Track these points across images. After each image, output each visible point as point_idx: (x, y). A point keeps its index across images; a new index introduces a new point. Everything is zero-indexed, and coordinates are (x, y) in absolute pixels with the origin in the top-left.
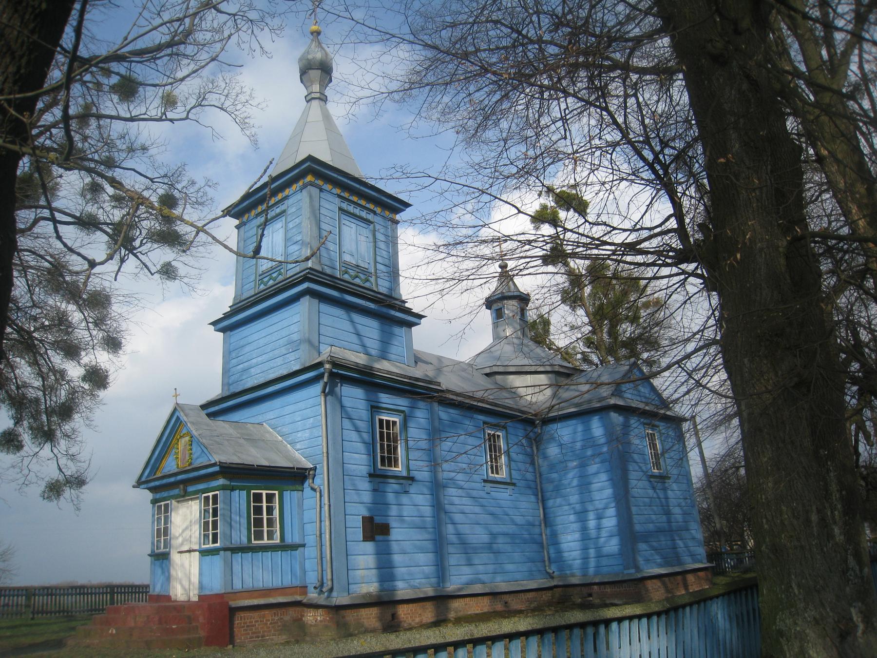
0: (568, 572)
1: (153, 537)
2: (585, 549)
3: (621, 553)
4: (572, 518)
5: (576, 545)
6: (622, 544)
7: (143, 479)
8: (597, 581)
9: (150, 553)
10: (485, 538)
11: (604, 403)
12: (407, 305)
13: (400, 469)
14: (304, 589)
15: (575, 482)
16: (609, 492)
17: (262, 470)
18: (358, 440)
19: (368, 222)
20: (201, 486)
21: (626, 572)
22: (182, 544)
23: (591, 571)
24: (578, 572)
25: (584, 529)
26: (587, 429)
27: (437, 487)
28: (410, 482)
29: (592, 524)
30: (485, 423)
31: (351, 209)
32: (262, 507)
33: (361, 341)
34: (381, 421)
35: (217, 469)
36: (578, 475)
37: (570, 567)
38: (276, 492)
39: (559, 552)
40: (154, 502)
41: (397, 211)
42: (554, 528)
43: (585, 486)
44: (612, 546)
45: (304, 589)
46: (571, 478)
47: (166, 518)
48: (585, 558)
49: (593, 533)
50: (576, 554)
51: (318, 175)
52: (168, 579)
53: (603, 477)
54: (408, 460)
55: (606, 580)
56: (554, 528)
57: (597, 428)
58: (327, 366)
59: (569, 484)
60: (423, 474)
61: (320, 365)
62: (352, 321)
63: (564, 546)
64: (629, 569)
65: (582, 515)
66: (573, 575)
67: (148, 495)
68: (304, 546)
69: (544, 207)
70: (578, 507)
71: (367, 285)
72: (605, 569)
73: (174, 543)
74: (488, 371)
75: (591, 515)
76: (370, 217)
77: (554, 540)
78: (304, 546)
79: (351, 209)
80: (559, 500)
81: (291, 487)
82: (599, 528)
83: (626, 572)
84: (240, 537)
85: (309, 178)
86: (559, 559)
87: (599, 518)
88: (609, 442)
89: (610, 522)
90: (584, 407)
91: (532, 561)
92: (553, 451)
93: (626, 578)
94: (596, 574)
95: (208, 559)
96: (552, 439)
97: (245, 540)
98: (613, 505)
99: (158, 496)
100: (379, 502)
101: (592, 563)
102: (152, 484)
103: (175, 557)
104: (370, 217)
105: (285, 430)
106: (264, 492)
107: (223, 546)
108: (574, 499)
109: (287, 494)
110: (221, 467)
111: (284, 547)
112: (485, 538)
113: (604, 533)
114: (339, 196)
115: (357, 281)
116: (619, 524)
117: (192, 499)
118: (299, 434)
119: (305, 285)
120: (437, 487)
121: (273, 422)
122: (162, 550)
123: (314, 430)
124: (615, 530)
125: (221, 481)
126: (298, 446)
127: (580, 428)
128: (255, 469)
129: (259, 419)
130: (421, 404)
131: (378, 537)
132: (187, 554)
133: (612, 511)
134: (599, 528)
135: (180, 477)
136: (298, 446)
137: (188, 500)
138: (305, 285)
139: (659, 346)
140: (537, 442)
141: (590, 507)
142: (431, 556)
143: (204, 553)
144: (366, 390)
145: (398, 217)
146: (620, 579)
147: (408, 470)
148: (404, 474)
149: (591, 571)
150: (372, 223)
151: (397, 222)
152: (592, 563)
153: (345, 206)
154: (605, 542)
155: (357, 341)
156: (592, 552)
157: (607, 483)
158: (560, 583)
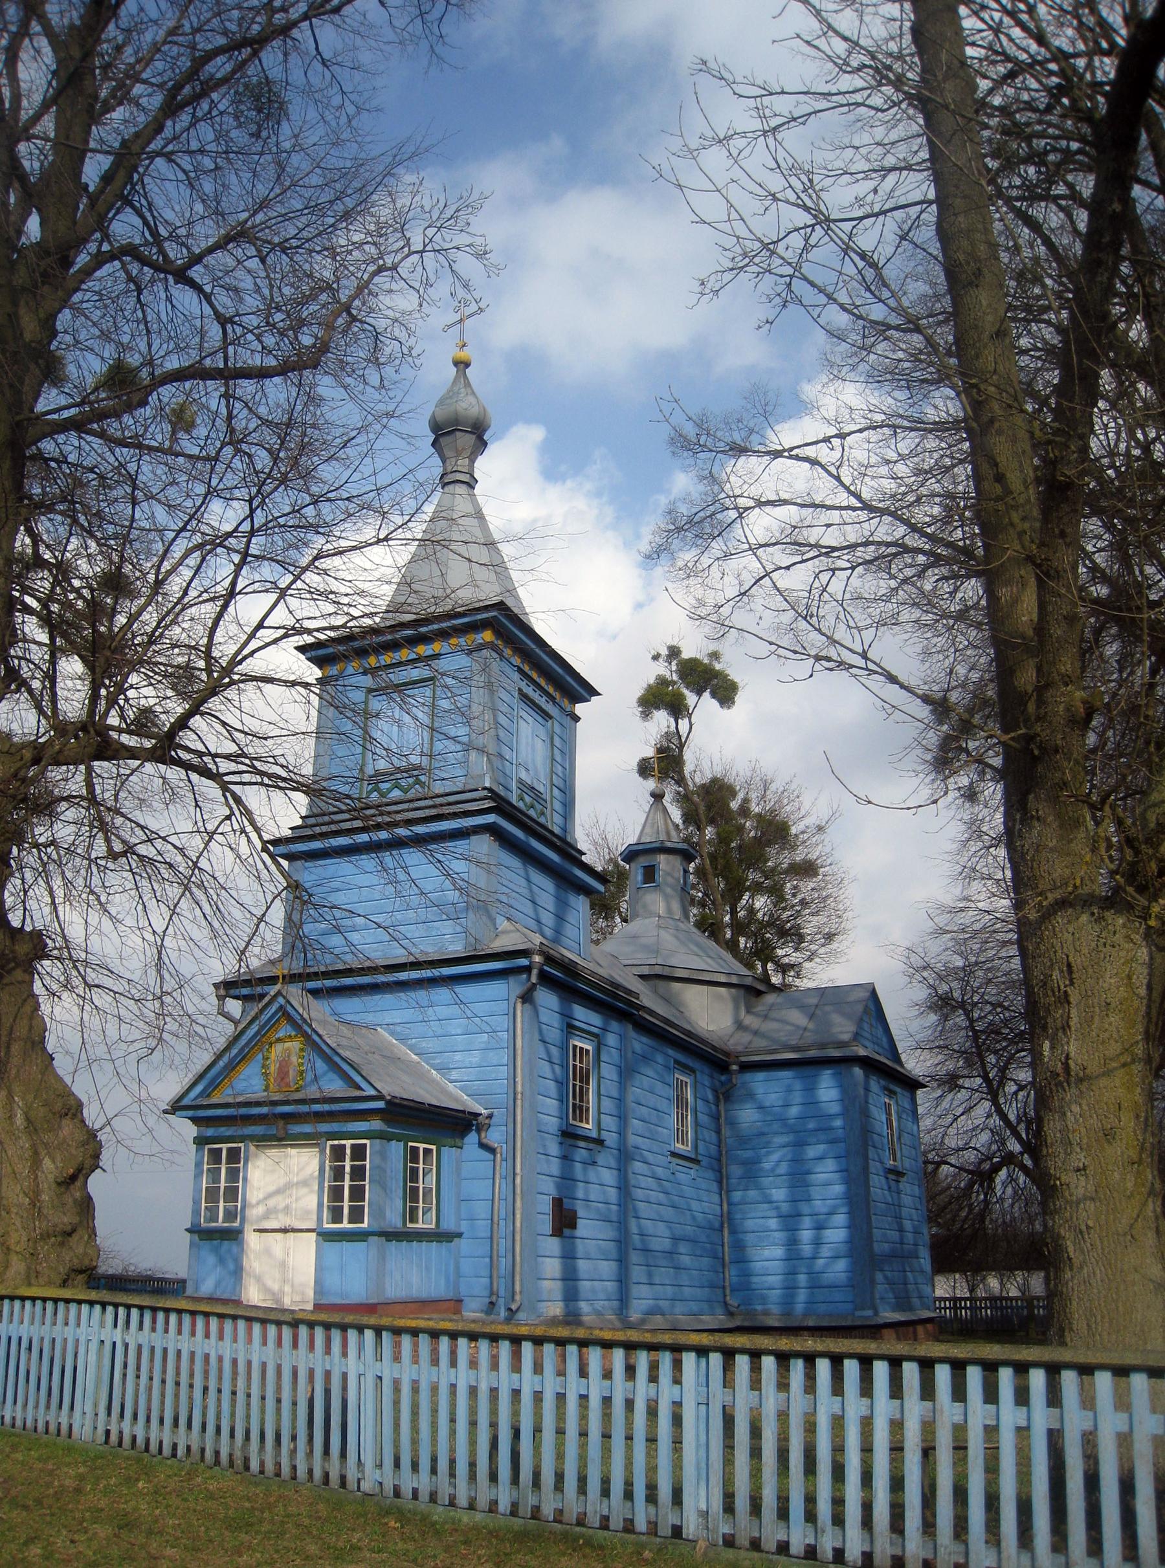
0: (759, 1308)
1: (196, 1202)
2: (791, 1273)
3: (851, 1285)
4: (773, 1223)
5: (777, 1266)
6: (852, 1270)
7: (185, 1102)
8: (811, 1323)
9: (189, 1226)
10: (666, 1244)
11: (846, 1052)
12: (583, 858)
13: (589, 1126)
14: (456, 1304)
15: (783, 1168)
16: (838, 1189)
17: (405, 1106)
18: (549, 1075)
19: (546, 716)
20: (335, 1127)
21: (858, 1313)
22: (266, 1216)
23: (799, 1308)
24: (775, 1309)
25: (792, 1243)
26: (810, 1089)
27: (625, 1156)
28: (599, 1148)
29: (806, 1235)
30: (677, 1062)
31: (536, 696)
32: (352, 1159)
33: (535, 910)
34: (575, 1047)
35: (381, 1104)
36: (789, 1157)
37: (764, 1299)
38: (434, 1147)
39: (746, 1274)
40: (200, 1141)
41: (577, 699)
42: (741, 1236)
43: (799, 1178)
44: (838, 1270)
45: (456, 1304)
46: (775, 1160)
47: (233, 1175)
48: (790, 1288)
49: (807, 1250)
50: (775, 1280)
51: (500, 632)
52: (238, 1272)
53: (830, 1164)
54: (599, 1113)
55: (825, 1324)
56: (741, 1236)
57: (827, 1090)
58: (537, 959)
59: (773, 1170)
60: (611, 1139)
61: (524, 953)
62: (528, 880)
63: (757, 1266)
64: (863, 1309)
65: (790, 1221)
66: (766, 1313)
67: (190, 1130)
68: (460, 1235)
69: (662, 682)
70: (785, 1208)
71: (542, 820)
72: (822, 1308)
73: (254, 1213)
74: (646, 971)
75: (807, 1222)
76: (549, 708)
77: (741, 1257)
78: (460, 1235)
79: (536, 696)
80: (752, 1194)
81: (449, 1141)
82: (817, 1243)
83: (858, 1313)
84: (393, 1218)
85: (488, 636)
86: (744, 1286)
87: (819, 1227)
88: (845, 1113)
89: (836, 1235)
90: (812, 1053)
91: (712, 1286)
92: (747, 1116)
93: (859, 1323)
94: (806, 1315)
95: (333, 1248)
96: (751, 1096)
97: (399, 1224)
98: (844, 1209)
99: (210, 1132)
100: (567, 1179)
101: (802, 1296)
102: (201, 1113)
103: (252, 1240)
104: (549, 708)
105: (425, 1045)
106: (422, 1146)
107: (376, 1227)
108: (779, 1194)
109: (445, 1150)
110: (388, 1103)
111: (441, 1236)
112: (666, 1244)
113: (825, 1251)
114: (520, 671)
115: (532, 813)
116: (850, 1241)
117: (292, 1146)
118: (458, 1057)
119: (491, 818)
120: (625, 1156)
121: (398, 1029)
122: (220, 1223)
123: (491, 1054)
124: (843, 1248)
125: (376, 1124)
126: (454, 1075)
127: (798, 1085)
128: (424, 1111)
129: (369, 1018)
130: (615, 1025)
131: (567, 1232)
132: (279, 1235)
133: (840, 1219)
134: (817, 1243)
135: (317, 1107)
136: (454, 1075)
137: (286, 1146)
138: (491, 818)
139: (801, 938)
140: (725, 1095)
141: (804, 1208)
142: (613, 1265)
143: (327, 1236)
144: (560, 997)
145: (580, 709)
146: (849, 1323)
147: (600, 1129)
148: (594, 1135)
149: (799, 1308)
150: (551, 717)
151: (576, 719)
152: (802, 1296)
153: (529, 691)
154: (827, 1265)
155: (531, 912)
156: (802, 1279)
157: (837, 1176)
158: (746, 1324)
